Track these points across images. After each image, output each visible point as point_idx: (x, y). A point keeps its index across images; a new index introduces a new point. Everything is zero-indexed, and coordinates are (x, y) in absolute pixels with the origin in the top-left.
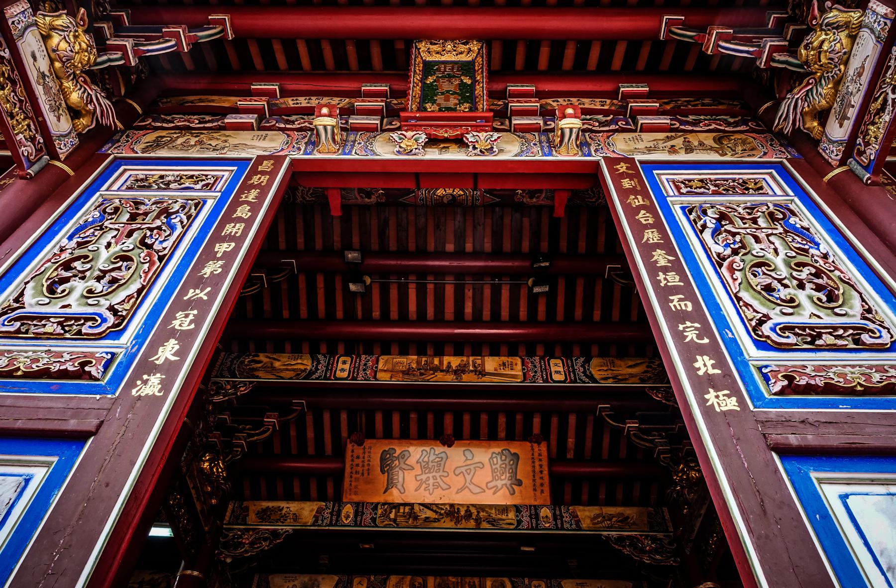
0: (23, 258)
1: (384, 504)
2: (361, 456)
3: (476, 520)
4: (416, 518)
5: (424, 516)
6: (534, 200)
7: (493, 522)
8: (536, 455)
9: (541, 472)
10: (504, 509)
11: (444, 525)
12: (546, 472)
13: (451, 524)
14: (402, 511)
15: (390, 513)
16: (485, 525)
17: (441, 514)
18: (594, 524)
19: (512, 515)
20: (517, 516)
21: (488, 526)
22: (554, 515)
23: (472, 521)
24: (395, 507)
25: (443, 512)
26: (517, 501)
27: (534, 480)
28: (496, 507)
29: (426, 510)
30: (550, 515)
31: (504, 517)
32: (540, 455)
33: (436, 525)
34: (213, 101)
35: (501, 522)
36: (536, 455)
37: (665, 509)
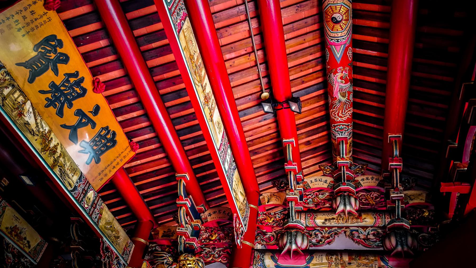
0: (237, 40)
1: (8, 73)
2: (36, 16)
3: (56, 161)
4: (21, 114)
5: (27, 119)
6: (340, 80)
7: (63, 173)
8: (123, 154)
9: (114, 167)
10: (75, 169)
11: (34, 143)
12: (115, 170)
13: (39, 147)
14: (16, 95)
15: (7, 87)
16: (57, 170)
17: (39, 131)
18: (105, 227)
19: (75, 178)
20: (77, 183)
21: (58, 173)
22: (94, 201)
23: (52, 158)
24: (13, 86)
25: (41, 130)
26: (84, 172)
27: (106, 168)
28: (72, 163)
29: (32, 115)
30: (92, 199)
31: (70, 175)
32: (125, 157)
33: (29, 136)
34: (396, 148)
35: (67, 178)
36: (123, 154)
37: (134, 246)
